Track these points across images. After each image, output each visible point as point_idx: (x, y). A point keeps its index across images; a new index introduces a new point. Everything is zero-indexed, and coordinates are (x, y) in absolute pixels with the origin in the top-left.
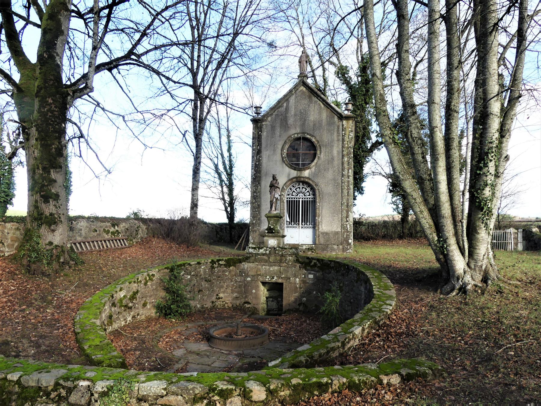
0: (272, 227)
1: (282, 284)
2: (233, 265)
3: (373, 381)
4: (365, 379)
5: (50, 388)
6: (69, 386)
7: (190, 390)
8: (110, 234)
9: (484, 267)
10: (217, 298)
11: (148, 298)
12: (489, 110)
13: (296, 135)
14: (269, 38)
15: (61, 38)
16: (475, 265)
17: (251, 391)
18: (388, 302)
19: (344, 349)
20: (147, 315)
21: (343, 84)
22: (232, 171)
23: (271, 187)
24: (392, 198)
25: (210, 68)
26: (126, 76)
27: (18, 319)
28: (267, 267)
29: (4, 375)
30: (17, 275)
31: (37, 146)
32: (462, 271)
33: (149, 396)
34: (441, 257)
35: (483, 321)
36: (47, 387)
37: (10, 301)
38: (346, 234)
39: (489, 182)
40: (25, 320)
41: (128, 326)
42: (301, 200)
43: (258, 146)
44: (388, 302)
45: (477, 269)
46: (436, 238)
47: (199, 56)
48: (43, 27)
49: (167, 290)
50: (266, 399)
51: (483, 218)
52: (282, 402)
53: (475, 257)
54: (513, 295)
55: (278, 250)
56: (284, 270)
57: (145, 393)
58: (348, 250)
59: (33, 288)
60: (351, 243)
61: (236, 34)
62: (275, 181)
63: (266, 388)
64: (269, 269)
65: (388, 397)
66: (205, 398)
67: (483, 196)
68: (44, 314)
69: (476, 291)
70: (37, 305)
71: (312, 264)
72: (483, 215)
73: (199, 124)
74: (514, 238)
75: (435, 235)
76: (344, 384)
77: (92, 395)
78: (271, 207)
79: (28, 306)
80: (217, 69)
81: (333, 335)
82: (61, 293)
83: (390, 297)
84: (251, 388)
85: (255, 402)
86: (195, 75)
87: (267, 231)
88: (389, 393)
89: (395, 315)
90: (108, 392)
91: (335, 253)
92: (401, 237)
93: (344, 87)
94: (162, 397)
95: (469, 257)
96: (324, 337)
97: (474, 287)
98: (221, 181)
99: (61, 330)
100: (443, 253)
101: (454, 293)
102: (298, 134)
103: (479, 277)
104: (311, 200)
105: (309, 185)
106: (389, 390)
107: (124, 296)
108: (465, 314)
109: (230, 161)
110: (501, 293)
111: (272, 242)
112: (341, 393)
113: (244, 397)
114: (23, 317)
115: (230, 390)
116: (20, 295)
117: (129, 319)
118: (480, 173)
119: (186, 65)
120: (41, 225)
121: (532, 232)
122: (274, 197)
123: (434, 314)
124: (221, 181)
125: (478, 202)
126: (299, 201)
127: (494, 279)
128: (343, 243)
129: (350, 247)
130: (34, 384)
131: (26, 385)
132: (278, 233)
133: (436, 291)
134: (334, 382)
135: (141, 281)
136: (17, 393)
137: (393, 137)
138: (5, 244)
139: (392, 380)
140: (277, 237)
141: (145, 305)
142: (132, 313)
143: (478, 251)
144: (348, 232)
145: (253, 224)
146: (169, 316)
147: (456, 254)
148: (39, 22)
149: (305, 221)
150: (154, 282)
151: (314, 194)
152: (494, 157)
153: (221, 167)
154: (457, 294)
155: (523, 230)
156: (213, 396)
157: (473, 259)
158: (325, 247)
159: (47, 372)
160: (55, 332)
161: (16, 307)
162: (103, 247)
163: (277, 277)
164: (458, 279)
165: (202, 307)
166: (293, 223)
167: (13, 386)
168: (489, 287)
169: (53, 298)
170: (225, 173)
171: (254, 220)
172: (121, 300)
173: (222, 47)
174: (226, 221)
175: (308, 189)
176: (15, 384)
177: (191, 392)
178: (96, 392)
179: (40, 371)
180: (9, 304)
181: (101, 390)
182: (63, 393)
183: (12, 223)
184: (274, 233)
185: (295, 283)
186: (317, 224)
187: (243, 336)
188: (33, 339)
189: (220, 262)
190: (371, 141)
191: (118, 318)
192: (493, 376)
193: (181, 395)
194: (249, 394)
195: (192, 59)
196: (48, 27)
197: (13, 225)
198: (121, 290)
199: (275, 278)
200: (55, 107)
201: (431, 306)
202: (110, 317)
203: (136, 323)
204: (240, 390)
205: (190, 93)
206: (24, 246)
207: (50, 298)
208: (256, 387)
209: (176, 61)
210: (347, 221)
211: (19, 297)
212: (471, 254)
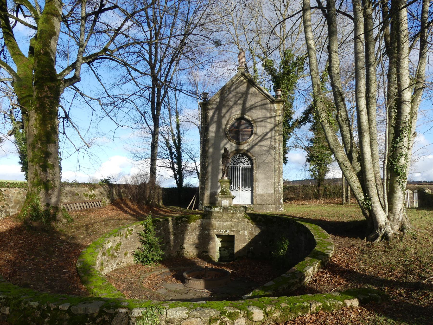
0: (224, 190)
1: (233, 236)
2: (193, 221)
3: (340, 304)
4: (334, 303)
5: (95, 315)
6: (111, 313)
7: (207, 313)
8: (88, 197)
9: (400, 219)
10: (180, 248)
11: (128, 249)
12: (402, 97)
13: (236, 116)
14: (216, 36)
15: (54, 37)
16: (393, 218)
17: (253, 313)
18: (329, 248)
19: (301, 284)
20: (128, 263)
21: (269, 74)
24: (310, 166)
25: (165, 61)
26: (98, 68)
27: (31, 266)
28: (221, 223)
29: (56, 306)
30: (23, 231)
31: (36, 125)
32: (383, 223)
33: (174, 319)
34: (367, 211)
35: (406, 261)
36: (93, 314)
37: (20, 252)
39: (404, 153)
40: (36, 267)
41: (114, 271)
42: (241, 168)
44: (329, 248)
45: (395, 221)
46: (363, 197)
47: (156, 51)
48: (39, 29)
49: (144, 243)
50: (264, 319)
51: (400, 181)
52: (275, 322)
53: (394, 211)
54: (424, 241)
55: (230, 209)
56: (235, 224)
57: (172, 317)
58: (280, 208)
59: (37, 242)
61: (186, 35)
63: (263, 310)
64: (223, 224)
65: (354, 316)
66: (218, 320)
67: (399, 164)
68: (50, 262)
69: (395, 238)
70: (43, 255)
71: (258, 219)
72: (399, 178)
73: (156, 105)
74: (410, 198)
75: (362, 195)
76: (320, 306)
77: (130, 319)
79: (35, 256)
80: (171, 62)
81: (290, 273)
82: (60, 246)
83: (330, 244)
84: (252, 311)
85: (255, 321)
86: (153, 68)
87: (220, 194)
88: (353, 313)
89: (336, 258)
90: (142, 317)
91: (270, 210)
92: (317, 197)
93: (270, 77)
94: (185, 319)
95: (389, 212)
96: (284, 275)
97: (394, 235)
98: (171, 153)
99: (67, 275)
100: (368, 209)
101: (378, 240)
103: (397, 227)
104: (249, 168)
106: (353, 311)
107: (111, 247)
108: (391, 255)
109: (179, 137)
110: (415, 239)
112: (318, 313)
113: (248, 318)
114: (34, 265)
115: (237, 313)
116: (28, 247)
117: (115, 266)
118: (397, 147)
119: (144, 59)
120: (40, 189)
121: (425, 193)
123: (366, 256)
124: (171, 153)
125: (396, 169)
127: (409, 229)
129: (282, 206)
130: (82, 312)
131: (76, 313)
133: (363, 239)
134: (312, 306)
135: (123, 235)
136: (67, 320)
137: (328, 119)
138: (10, 206)
139: (353, 303)
141: (126, 254)
142: (117, 261)
143: (396, 207)
144: (279, 194)
146: (146, 263)
147: (379, 209)
148: (36, 25)
149: (244, 185)
150: (133, 235)
151: (252, 164)
152: (407, 134)
153: (171, 142)
154: (381, 241)
155: (418, 191)
156: (224, 318)
157: (392, 213)
158: (262, 206)
159: (89, 303)
160: (63, 276)
161: (27, 257)
162: (84, 208)
163: (229, 230)
164: (381, 229)
165: (170, 256)
166: (234, 187)
167: (64, 314)
168: (405, 235)
169: (55, 249)
170: (175, 147)
172: (109, 251)
173: (174, 42)
174: (176, 186)
175: (247, 159)
176: (66, 313)
177: (208, 315)
178: (133, 317)
179: (84, 302)
180: (21, 254)
181: (137, 315)
182: (107, 318)
183: (15, 189)
185: (244, 235)
186: (255, 188)
187: (210, 278)
188: (47, 282)
189: (183, 219)
190: (292, 120)
191: (107, 265)
192: (425, 300)
193: (200, 318)
194: (251, 315)
195: (150, 55)
196: (44, 29)
197: (15, 190)
198: (108, 242)
199: (228, 231)
200: (50, 94)
201: (362, 250)
202: (102, 264)
203: (120, 269)
204: (244, 312)
205: (148, 81)
206: (27, 207)
207: (52, 249)
208: (256, 310)
209: (135, 56)
210: (279, 185)
211: (27, 249)
212: (391, 210)
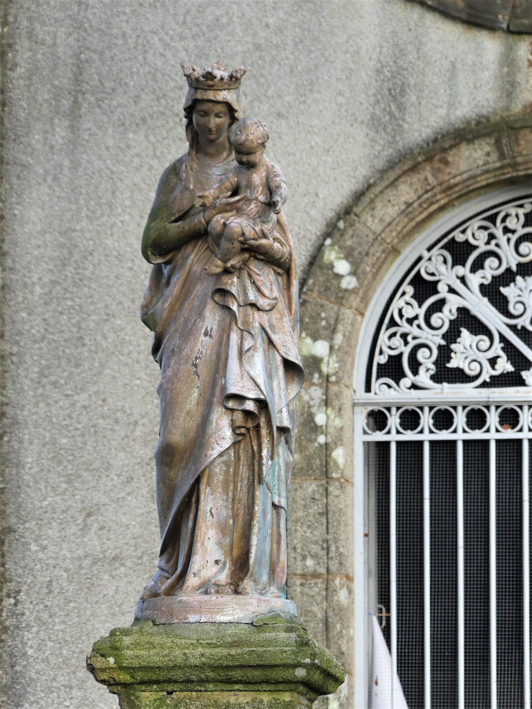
23: (162, 248)
62: (221, 170)
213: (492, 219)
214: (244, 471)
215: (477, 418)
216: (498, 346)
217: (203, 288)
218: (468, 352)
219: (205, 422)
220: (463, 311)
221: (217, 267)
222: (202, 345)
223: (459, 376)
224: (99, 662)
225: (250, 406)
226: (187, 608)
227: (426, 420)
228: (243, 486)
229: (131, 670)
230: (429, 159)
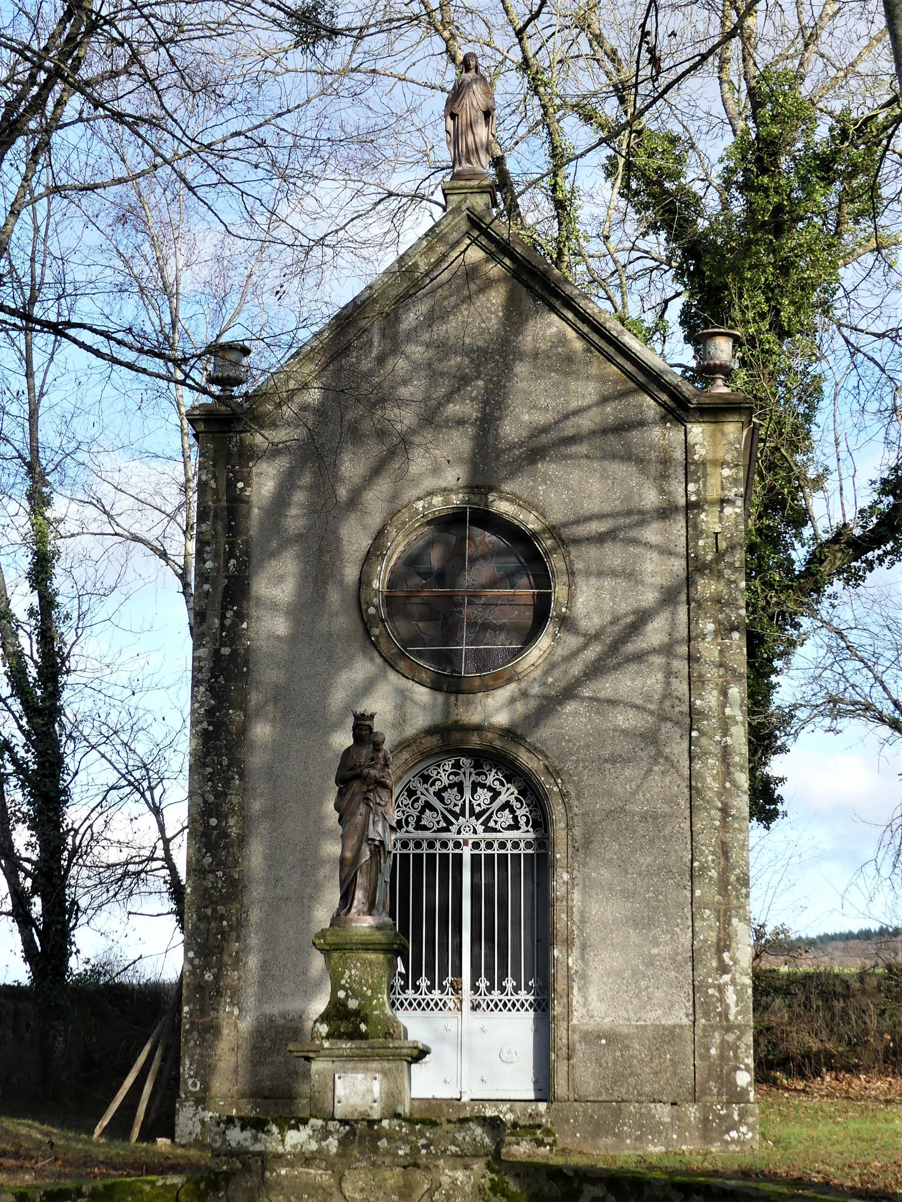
0: (353, 1004)
13: (437, 500)
21: (654, 227)
22: (54, 693)
23: (343, 781)
38: (717, 1037)
42: (467, 853)
43: (230, 555)
55: (390, 1137)
58: (734, 1126)
60: (745, 1092)
62: (366, 752)
78: (347, 898)
87: (324, 1029)
93: (657, 243)
102: (445, 491)
104: (522, 851)
105: (513, 773)
109: (46, 635)
111: (356, 1089)
122: (363, 837)
126: (458, 858)
128: (706, 1091)
129: (743, 1114)
132: (388, 1035)
140: (381, 1057)
144: (729, 1029)
145: (200, 987)
149: (492, 970)
151: (541, 822)
158: (608, 1114)
166: (424, 982)
171: (207, 966)
174: (19, 973)
184: (364, 1036)
186: (560, 986)
190: (807, 532)
210: (723, 969)
213: (439, 766)
214: (374, 868)
215: (431, 845)
216: (499, 828)
217: (358, 797)
218: (428, 818)
219: (359, 849)
220: (427, 802)
221: (365, 789)
222: (359, 819)
223: (425, 828)
224: (317, 941)
225: (377, 843)
226: (351, 920)
227: (411, 845)
228: (373, 874)
229: (329, 945)
230: (415, 742)
